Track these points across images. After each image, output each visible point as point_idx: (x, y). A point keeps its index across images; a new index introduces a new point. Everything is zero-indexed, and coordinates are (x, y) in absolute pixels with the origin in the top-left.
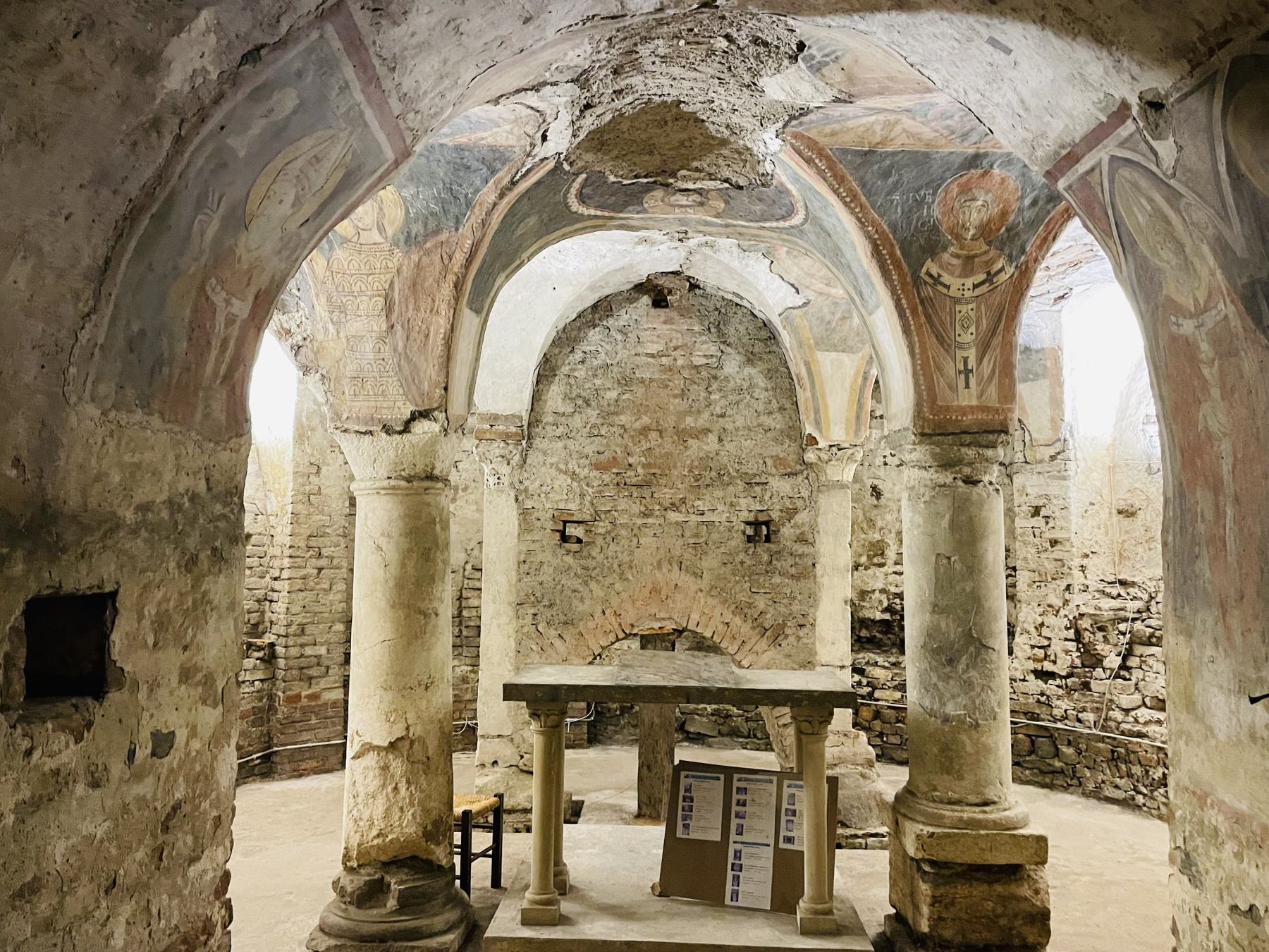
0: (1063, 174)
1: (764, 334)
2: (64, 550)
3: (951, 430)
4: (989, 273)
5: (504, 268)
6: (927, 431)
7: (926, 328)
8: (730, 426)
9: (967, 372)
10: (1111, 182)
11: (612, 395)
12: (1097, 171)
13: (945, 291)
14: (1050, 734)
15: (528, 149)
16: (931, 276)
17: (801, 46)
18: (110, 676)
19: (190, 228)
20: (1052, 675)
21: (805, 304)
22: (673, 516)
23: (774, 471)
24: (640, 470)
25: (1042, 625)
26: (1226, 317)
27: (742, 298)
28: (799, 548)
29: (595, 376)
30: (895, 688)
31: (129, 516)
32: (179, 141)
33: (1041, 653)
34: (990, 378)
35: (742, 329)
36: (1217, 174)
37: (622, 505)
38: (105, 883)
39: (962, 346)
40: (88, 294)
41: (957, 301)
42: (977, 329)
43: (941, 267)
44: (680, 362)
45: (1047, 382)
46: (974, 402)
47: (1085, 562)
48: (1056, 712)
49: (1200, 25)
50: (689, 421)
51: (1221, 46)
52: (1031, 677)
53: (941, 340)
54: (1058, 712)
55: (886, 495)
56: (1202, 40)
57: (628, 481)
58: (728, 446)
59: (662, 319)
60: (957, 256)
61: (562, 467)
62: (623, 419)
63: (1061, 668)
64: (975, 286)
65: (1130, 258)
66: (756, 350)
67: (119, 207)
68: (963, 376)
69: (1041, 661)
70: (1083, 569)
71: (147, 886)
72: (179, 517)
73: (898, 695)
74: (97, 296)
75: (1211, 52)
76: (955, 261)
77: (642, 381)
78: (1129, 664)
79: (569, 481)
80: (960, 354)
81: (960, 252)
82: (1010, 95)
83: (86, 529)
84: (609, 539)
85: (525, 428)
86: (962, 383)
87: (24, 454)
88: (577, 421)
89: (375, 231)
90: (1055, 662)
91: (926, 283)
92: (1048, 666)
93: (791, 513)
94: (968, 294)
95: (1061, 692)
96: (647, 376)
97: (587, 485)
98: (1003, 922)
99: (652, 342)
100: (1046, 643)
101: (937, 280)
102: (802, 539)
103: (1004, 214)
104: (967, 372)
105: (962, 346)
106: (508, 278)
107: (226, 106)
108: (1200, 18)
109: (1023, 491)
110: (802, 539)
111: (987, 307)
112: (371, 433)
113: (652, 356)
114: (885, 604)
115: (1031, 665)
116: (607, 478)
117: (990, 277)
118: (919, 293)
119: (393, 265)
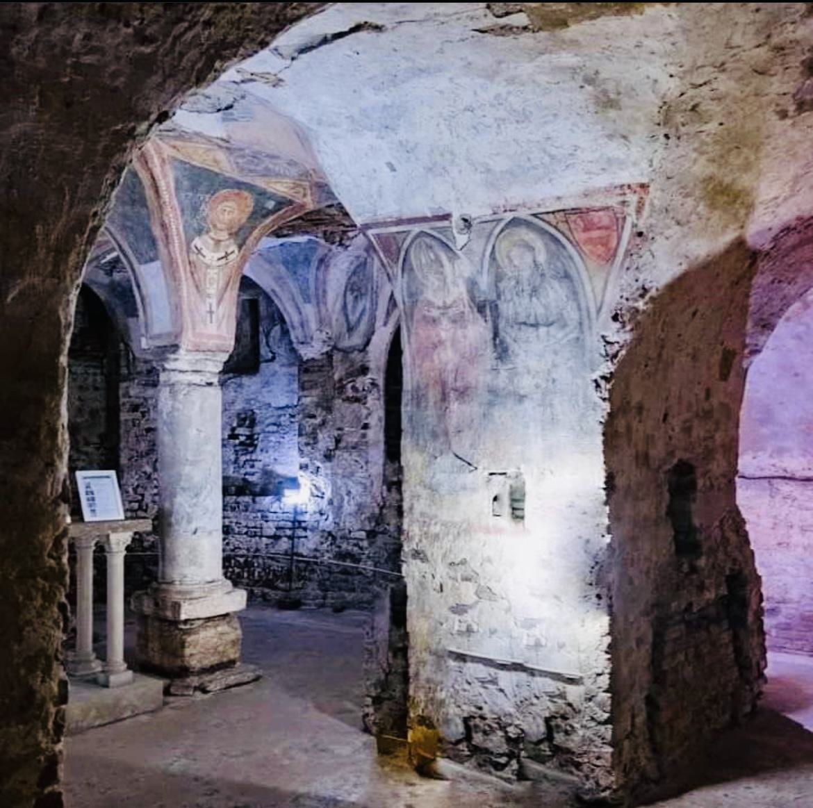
3: (203, 348)
6: (190, 348)
7: (191, 281)
9: (211, 312)
10: (412, 242)
25: (138, 486)
26: (463, 313)
34: (223, 317)
36: (484, 255)
39: (209, 296)
41: (208, 266)
43: (203, 243)
46: (215, 332)
48: (146, 544)
49: (506, 201)
56: (504, 206)
60: (213, 239)
64: (219, 259)
75: (505, 211)
80: (208, 300)
82: (125, 715)
86: (208, 319)
98: (221, 649)
100: (140, 498)
101: (199, 251)
104: (211, 312)
105: (209, 296)
109: (127, 395)
117: (227, 255)
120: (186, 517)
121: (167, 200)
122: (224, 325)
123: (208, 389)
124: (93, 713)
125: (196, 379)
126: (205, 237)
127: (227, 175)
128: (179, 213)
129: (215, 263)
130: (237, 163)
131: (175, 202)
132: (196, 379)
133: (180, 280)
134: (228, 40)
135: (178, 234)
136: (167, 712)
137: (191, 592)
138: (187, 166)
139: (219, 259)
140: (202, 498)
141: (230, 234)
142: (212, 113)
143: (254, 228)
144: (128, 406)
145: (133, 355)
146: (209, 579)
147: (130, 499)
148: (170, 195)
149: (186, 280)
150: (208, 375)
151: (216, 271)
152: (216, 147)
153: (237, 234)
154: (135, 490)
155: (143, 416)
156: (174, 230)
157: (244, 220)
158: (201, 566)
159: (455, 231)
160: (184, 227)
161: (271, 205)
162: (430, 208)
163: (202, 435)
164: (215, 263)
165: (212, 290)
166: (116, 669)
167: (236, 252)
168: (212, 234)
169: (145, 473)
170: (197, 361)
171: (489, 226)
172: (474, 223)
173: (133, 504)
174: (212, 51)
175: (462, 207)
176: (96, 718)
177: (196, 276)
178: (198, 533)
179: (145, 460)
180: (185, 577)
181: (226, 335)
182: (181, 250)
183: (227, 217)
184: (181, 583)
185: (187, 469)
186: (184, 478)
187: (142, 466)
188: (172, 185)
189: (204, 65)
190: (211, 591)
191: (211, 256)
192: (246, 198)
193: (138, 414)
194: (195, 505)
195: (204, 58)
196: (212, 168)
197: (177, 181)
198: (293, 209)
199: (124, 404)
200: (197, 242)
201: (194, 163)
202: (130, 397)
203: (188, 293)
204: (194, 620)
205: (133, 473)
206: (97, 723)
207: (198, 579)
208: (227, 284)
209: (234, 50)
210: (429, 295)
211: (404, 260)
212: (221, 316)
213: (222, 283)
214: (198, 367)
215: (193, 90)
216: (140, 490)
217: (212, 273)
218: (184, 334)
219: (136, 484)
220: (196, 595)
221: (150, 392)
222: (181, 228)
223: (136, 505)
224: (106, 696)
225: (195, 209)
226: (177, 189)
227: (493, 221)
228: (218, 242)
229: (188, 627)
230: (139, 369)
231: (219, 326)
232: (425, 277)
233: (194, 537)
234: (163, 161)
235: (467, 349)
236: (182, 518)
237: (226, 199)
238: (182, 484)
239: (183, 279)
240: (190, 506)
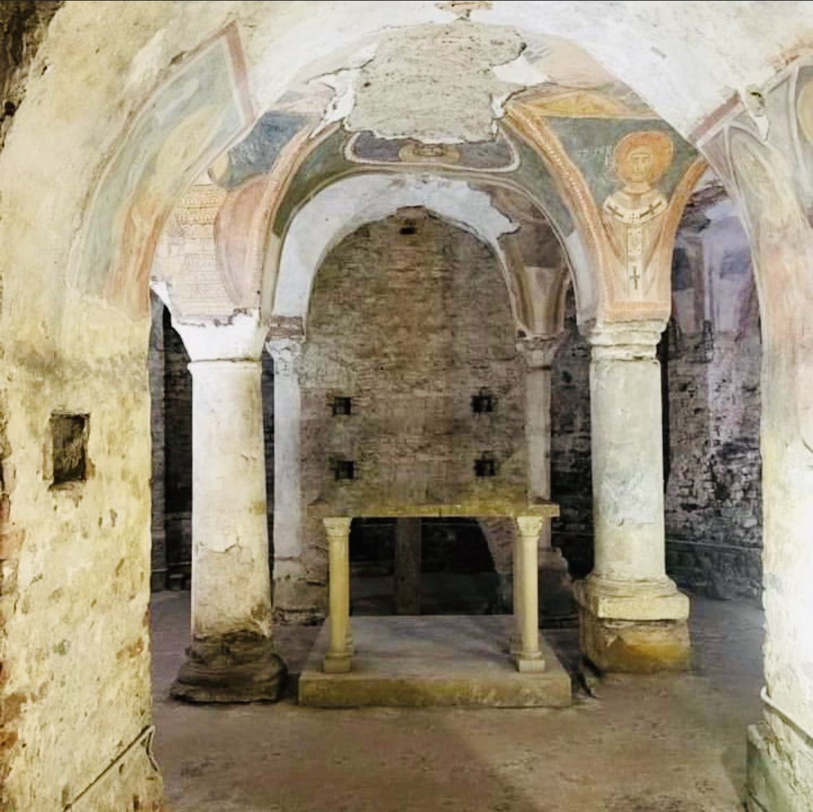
0: (700, 137)
1: (486, 253)
2: (66, 382)
4: (651, 206)
5: (296, 204)
6: (608, 320)
7: (607, 246)
8: (460, 323)
9: (636, 278)
11: (370, 301)
12: (721, 137)
14: (691, 549)
15: (322, 114)
16: (610, 208)
17: (524, 47)
18: (88, 468)
19: (127, 175)
20: (694, 507)
21: (517, 231)
22: (419, 393)
23: (493, 357)
24: (393, 359)
25: (687, 471)
27: (468, 226)
28: (513, 415)
29: (357, 286)
30: (582, 522)
31: (93, 366)
32: (131, 114)
33: (686, 491)
34: (653, 280)
35: (468, 249)
36: (792, 139)
37: (381, 384)
38: (92, 601)
39: (632, 259)
40: (78, 216)
41: (628, 226)
44: (422, 275)
45: (691, 290)
47: (718, 423)
49: (781, 46)
50: (430, 320)
51: (793, 59)
52: (679, 510)
53: (617, 253)
54: (697, 533)
55: (575, 378)
56: (783, 56)
57: (385, 366)
58: (459, 338)
59: (408, 242)
60: (629, 194)
61: (333, 355)
62: (379, 319)
63: (701, 502)
64: (641, 216)
65: (742, 193)
66: (480, 266)
67: (97, 158)
68: (633, 280)
69: (687, 497)
70: (717, 429)
71: (110, 607)
72: (116, 369)
73: (583, 527)
74: (82, 216)
76: (627, 198)
77: (393, 290)
78: (749, 496)
79: (339, 367)
80: (631, 264)
82: (529, 704)
83: (75, 371)
84: (370, 409)
85: (304, 326)
86: (632, 285)
87: (47, 320)
88: (345, 321)
89: (206, 176)
90: (696, 497)
91: (607, 213)
92: (692, 501)
93: (506, 389)
95: (700, 519)
96: (397, 286)
97: (354, 370)
99: (401, 260)
100: (690, 483)
101: (614, 211)
102: (514, 408)
103: (57, 602)
105: (632, 259)
106: (300, 209)
107: (159, 92)
108: (781, 42)
110: (514, 408)
111: (650, 231)
112: (203, 325)
113: (400, 271)
114: (573, 461)
115: (680, 500)
116: (367, 364)
117: (651, 211)
118: (602, 220)
119: (220, 199)
120: (612, 507)
121: (561, 164)
122: (654, 290)
123: (640, 365)
124: (493, 693)
125: (621, 353)
127: (621, 118)
129: (637, 221)
130: (622, 102)
131: (571, 164)
132: (621, 353)
133: (594, 247)
134: (22, 10)
135: (585, 197)
136: (570, 713)
137: (617, 589)
138: (568, 122)
139: (641, 216)
140: (630, 486)
142: (516, 58)
143: (681, 174)
144: (676, 386)
145: (680, 331)
146: (641, 577)
147: (680, 484)
148: (562, 158)
149: (602, 246)
150: (636, 348)
151: (639, 230)
152: (583, 92)
153: (661, 182)
154: (685, 474)
155: (692, 396)
156: (579, 194)
158: (629, 562)
159: (751, 114)
160: (591, 188)
162: (724, 96)
163: (629, 415)
164: (637, 221)
165: (637, 252)
166: (527, 654)
167: (664, 202)
168: (627, 189)
169: (695, 456)
170: (620, 333)
171: (780, 94)
172: (764, 93)
173: (683, 490)
174: (15, 28)
175: (743, 78)
176: (496, 699)
177: (613, 239)
178: (625, 525)
179: (693, 443)
180: (612, 571)
181: (657, 301)
182: (592, 214)
183: (642, 166)
184: (608, 577)
185: (612, 453)
186: (608, 463)
187: (691, 450)
188: (560, 146)
189: (14, 41)
190: (638, 591)
191: (629, 214)
192: (659, 139)
193: (687, 393)
194: (622, 493)
195: (10, 36)
196: (598, 116)
197: (562, 140)
199: (672, 384)
200: (611, 201)
201: (574, 116)
202: (678, 376)
203: (605, 260)
204: (621, 620)
205: (683, 456)
206: (498, 704)
207: (627, 576)
208: (655, 246)
209: (32, 17)
210: (767, 215)
211: (735, 173)
212: (649, 280)
213: (648, 243)
214: (623, 341)
215: (18, 72)
216: (690, 475)
217: (635, 232)
218: (599, 308)
219: (685, 468)
220: (620, 593)
221: (697, 369)
222: (587, 191)
223: (686, 491)
224: (511, 679)
225: (599, 167)
227: (782, 83)
228: (637, 196)
229: (613, 626)
230: (686, 345)
231: (646, 293)
232: (757, 190)
233: (621, 528)
234: (538, 123)
236: (609, 507)
237: (633, 145)
238: (607, 470)
239: (598, 246)
240: (616, 495)
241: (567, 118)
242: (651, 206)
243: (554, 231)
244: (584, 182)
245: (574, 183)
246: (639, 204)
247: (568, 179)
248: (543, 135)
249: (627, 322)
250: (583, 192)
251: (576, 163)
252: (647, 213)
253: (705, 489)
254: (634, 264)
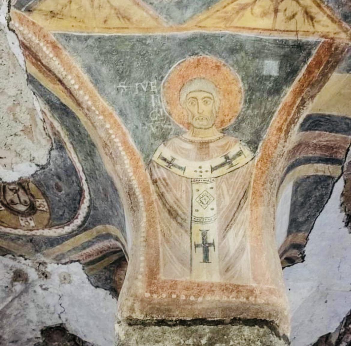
3: (177, 315)
4: (227, 158)
6: (138, 315)
7: (158, 205)
13: (180, 172)
42: (218, 205)
46: (216, 278)
60: (192, 142)
68: (200, 250)
76: (189, 146)
81: (193, 139)
91: (159, 166)
94: (207, 175)
104: (206, 247)
118: (151, 175)
126: (176, 142)
128: (119, 120)
131: (103, 102)
138: (90, 42)
139: (213, 169)
141: (223, 131)
153: (237, 128)
157: (240, 107)
161: (271, 67)
164: (207, 175)
183: (206, 109)
188: (86, 77)
191: (192, 165)
198: (318, 63)
200: (165, 151)
213: (227, 201)
222: (131, 141)
225: (144, 110)
226: (96, 82)
228: (204, 145)
235: (55, 22)
237: (185, 80)
241: (89, 37)
242: (227, 158)
243: (126, 257)
244: (125, 130)
245: (111, 131)
246: (208, 154)
247: (103, 126)
248: (62, 61)
249: (183, 322)
250: (125, 142)
251: (113, 103)
252: (222, 165)
253: (170, 42)
254: (204, 227)
